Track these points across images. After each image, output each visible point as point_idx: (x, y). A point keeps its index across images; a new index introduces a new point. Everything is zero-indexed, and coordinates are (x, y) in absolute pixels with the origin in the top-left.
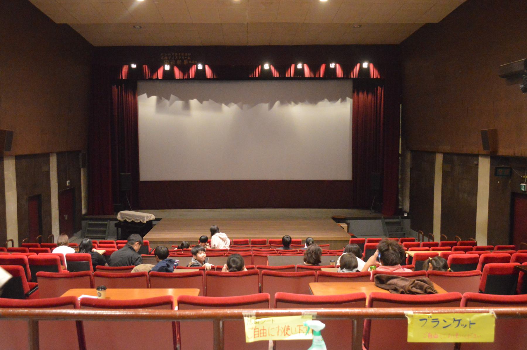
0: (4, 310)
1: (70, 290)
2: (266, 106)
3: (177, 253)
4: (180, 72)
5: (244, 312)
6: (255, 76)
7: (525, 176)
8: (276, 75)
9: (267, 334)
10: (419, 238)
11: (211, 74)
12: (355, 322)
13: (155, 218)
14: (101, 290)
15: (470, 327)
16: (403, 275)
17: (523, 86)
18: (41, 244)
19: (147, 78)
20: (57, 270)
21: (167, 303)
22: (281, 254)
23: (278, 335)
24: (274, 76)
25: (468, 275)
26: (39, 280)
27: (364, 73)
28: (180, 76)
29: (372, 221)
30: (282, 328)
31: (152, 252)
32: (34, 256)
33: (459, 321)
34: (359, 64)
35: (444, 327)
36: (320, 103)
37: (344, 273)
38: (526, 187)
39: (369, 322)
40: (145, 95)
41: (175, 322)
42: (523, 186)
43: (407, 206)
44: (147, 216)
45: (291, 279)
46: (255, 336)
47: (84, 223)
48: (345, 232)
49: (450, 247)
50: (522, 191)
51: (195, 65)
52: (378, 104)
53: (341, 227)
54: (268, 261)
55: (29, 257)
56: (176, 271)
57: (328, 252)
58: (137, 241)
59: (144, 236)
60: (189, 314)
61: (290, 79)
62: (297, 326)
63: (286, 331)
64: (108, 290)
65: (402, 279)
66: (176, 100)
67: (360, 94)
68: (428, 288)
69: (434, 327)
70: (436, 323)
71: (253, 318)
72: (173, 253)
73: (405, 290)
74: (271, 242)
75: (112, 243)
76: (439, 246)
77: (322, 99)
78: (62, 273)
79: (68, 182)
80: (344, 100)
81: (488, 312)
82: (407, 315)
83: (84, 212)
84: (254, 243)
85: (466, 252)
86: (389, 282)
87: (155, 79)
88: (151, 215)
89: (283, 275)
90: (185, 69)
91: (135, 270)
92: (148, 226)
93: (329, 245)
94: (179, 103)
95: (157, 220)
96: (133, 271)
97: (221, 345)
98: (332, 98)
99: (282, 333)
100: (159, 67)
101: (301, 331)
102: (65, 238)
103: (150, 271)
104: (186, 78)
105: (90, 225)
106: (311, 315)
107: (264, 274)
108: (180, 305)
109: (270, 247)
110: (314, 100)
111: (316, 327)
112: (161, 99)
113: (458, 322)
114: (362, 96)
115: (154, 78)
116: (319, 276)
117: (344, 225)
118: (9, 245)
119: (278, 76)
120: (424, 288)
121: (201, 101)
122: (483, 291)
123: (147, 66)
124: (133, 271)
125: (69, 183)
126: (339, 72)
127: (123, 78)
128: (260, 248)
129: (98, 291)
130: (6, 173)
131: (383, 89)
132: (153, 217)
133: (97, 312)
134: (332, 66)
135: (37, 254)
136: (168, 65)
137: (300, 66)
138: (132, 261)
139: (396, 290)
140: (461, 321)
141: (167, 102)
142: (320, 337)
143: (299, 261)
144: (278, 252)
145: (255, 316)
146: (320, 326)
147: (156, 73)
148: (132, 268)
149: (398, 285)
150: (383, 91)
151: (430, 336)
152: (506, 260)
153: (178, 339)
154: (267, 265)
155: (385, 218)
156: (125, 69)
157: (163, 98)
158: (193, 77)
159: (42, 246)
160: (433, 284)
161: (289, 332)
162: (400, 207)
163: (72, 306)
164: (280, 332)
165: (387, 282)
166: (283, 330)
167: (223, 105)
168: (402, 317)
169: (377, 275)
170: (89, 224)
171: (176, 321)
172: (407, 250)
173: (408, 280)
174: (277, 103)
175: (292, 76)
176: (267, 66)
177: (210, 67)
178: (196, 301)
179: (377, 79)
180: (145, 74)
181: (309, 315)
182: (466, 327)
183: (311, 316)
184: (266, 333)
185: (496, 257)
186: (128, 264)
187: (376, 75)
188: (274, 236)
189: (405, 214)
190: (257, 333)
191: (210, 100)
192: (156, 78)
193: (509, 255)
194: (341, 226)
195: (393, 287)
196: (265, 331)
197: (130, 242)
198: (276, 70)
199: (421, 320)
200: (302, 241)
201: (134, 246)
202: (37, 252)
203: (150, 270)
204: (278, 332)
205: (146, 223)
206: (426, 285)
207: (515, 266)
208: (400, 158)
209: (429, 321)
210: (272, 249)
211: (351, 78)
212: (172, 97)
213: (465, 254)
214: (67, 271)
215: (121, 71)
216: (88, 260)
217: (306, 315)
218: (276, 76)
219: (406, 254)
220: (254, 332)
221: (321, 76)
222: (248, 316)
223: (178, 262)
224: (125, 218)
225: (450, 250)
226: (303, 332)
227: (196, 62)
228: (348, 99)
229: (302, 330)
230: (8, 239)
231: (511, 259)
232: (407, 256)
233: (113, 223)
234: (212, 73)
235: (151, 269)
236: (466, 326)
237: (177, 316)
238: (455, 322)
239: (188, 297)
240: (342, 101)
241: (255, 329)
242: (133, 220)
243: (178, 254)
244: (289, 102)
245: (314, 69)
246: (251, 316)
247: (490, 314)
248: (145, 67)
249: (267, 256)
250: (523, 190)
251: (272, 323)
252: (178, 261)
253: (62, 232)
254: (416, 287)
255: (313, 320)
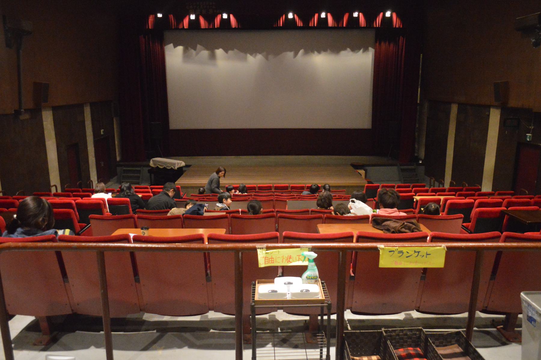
0: (79, 244)
1: (119, 230)
2: (291, 54)
3: (207, 197)
4: (205, 21)
5: (257, 245)
6: (279, 26)
7: (531, 127)
8: (299, 24)
9: (275, 261)
10: (430, 183)
11: (236, 24)
12: (341, 253)
13: (185, 165)
14: (145, 230)
15: (426, 257)
16: (396, 218)
17: (534, 40)
18: (83, 189)
19: (173, 28)
20: (101, 212)
21: (200, 239)
22: (300, 199)
23: (282, 262)
24: (298, 25)
25: (452, 218)
26: (92, 221)
27: (387, 22)
28: (205, 26)
29: (389, 167)
30: (286, 257)
31: (183, 196)
32: (80, 200)
33: (419, 252)
34: (382, 13)
35: (407, 257)
36: (343, 53)
37: (356, 216)
38: (531, 137)
39: (356, 253)
40: (171, 45)
41: (206, 253)
42: (529, 136)
43: (422, 154)
44: (178, 163)
45: (302, 221)
46: (266, 263)
47: (119, 169)
48: (362, 178)
49: (454, 193)
50: (528, 141)
51: (220, 14)
52: (400, 53)
53: (358, 174)
54: (287, 206)
55: (76, 201)
56: (206, 214)
57: (343, 196)
58: (172, 189)
59: (176, 181)
60: (216, 247)
61: (313, 28)
62: (297, 256)
63: (288, 259)
64: (150, 229)
65: (395, 221)
66: (203, 50)
67: (382, 44)
68: (416, 229)
69: (400, 257)
70: (401, 254)
71: (264, 250)
72: (203, 197)
73: (395, 230)
74: (293, 188)
75: (147, 188)
76: (429, 191)
77: (344, 49)
78: (106, 215)
79: (102, 130)
80: (366, 49)
81: (441, 246)
82: (380, 248)
83: (118, 159)
84: (277, 188)
85: (466, 198)
86: (384, 224)
87: (181, 29)
88: (182, 163)
89: (295, 217)
90: (210, 19)
91: (171, 213)
92: (179, 172)
93: (345, 190)
94: (205, 53)
95: (187, 166)
96: (169, 214)
97: (241, 269)
98: (355, 48)
99: (286, 261)
100: (184, 17)
101: (300, 259)
102: (102, 185)
103: (183, 214)
104: (212, 27)
105: (125, 171)
106: (307, 248)
107: (281, 217)
108: (210, 241)
109: (291, 192)
110: (336, 49)
111: (310, 256)
112: (188, 49)
113: (417, 253)
114: (384, 46)
115: (180, 28)
116: (326, 219)
117: (362, 172)
118: (53, 190)
119: (302, 25)
120: (412, 229)
121: (226, 51)
122: (473, 231)
123: (173, 16)
124: (169, 214)
125: (103, 132)
126: (330, 21)
127: (150, 28)
128: (282, 193)
129: (142, 231)
130: (44, 123)
131: (405, 39)
132: (183, 164)
133: (147, 246)
134: (356, 15)
135: (82, 199)
136: (193, 14)
137: (323, 15)
138: (168, 206)
139: (388, 230)
140: (420, 253)
141: (193, 52)
142: (313, 264)
143: (312, 205)
144: (298, 197)
145: (265, 248)
146: (314, 255)
147: (182, 23)
148: (168, 212)
149: (391, 226)
150: (405, 40)
151: (396, 263)
152: (499, 204)
153: (209, 266)
154: (287, 209)
155: (401, 165)
156: (151, 19)
157: (189, 48)
158: (218, 26)
159: (83, 191)
160: (420, 225)
161: (291, 260)
162: (416, 155)
163: (127, 241)
164: (284, 260)
165: (382, 224)
166: (286, 259)
167: (248, 55)
168: (376, 249)
169: (374, 218)
170: (124, 170)
171: (206, 252)
172: (415, 196)
173: (399, 222)
174: (301, 52)
175: (315, 26)
176: (290, 16)
177: (235, 16)
178: (222, 238)
179: (399, 28)
180: (171, 21)
181: (306, 248)
182: (424, 257)
183: (307, 249)
184: (274, 261)
185: (489, 202)
186: (165, 208)
187: (398, 24)
188: (297, 182)
189: (420, 161)
190: (267, 260)
191: (235, 50)
192: (182, 27)
193: (502, 200)
194: (359, 173)
195: (386, 228)
196: (273, 260)
197: (166, 189)
198: (300, 20)
199: (390, 252)
200: (321, 186)
201: (169, 193)
202: (82, 197)
203: (183, 213)
204: (283, 260)
205: (177, 169)
206: (414, 226)
207: (501, 211)
208: (418, 107)
209: (396, 253)
210: (293, 194)
211: (373, 28)
212: (199, 46)
213: (465, 199)
214: (110, 213)
215: (147, 24)
216: (128, 204)
217: (304, 248)
218: (299, 26)
219: (413, 199)
220: (265, 260)
221: (344, 26)
222: (260, 249)
223: (208, 206)
224: (157, 165)
225: (455, 195)
226: (302, 260)
227: (221, 11)
228: (370, 49)
229: (301, 259)
230: (52, 184)
231: (503, 204)
232: (415, 200)
233: (146, 169)
234: (237, 24)
235: (184, 212)
236: (423, 256)
237: (208, 248)
238: (415, 253)
239: (215, 235)
240: (364, 52)
241: (265, 258)
242: (165, 166)
243: (207, 199)
244: (312, 51)
245: (337, 18)
246: (262, 248)
247: (442, 247)
248: (171, 17)
249: (286, 201)
250: (528, 140)
251: (279, 253)
252: (207, 205)
253: (100, 179)
254: (405, 228)
255: (309, 251)
